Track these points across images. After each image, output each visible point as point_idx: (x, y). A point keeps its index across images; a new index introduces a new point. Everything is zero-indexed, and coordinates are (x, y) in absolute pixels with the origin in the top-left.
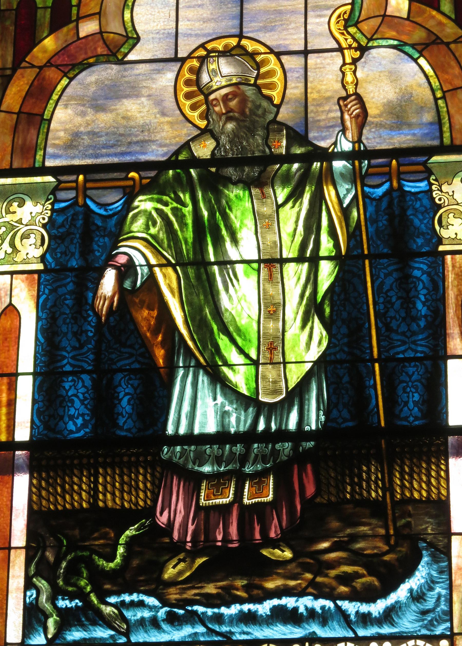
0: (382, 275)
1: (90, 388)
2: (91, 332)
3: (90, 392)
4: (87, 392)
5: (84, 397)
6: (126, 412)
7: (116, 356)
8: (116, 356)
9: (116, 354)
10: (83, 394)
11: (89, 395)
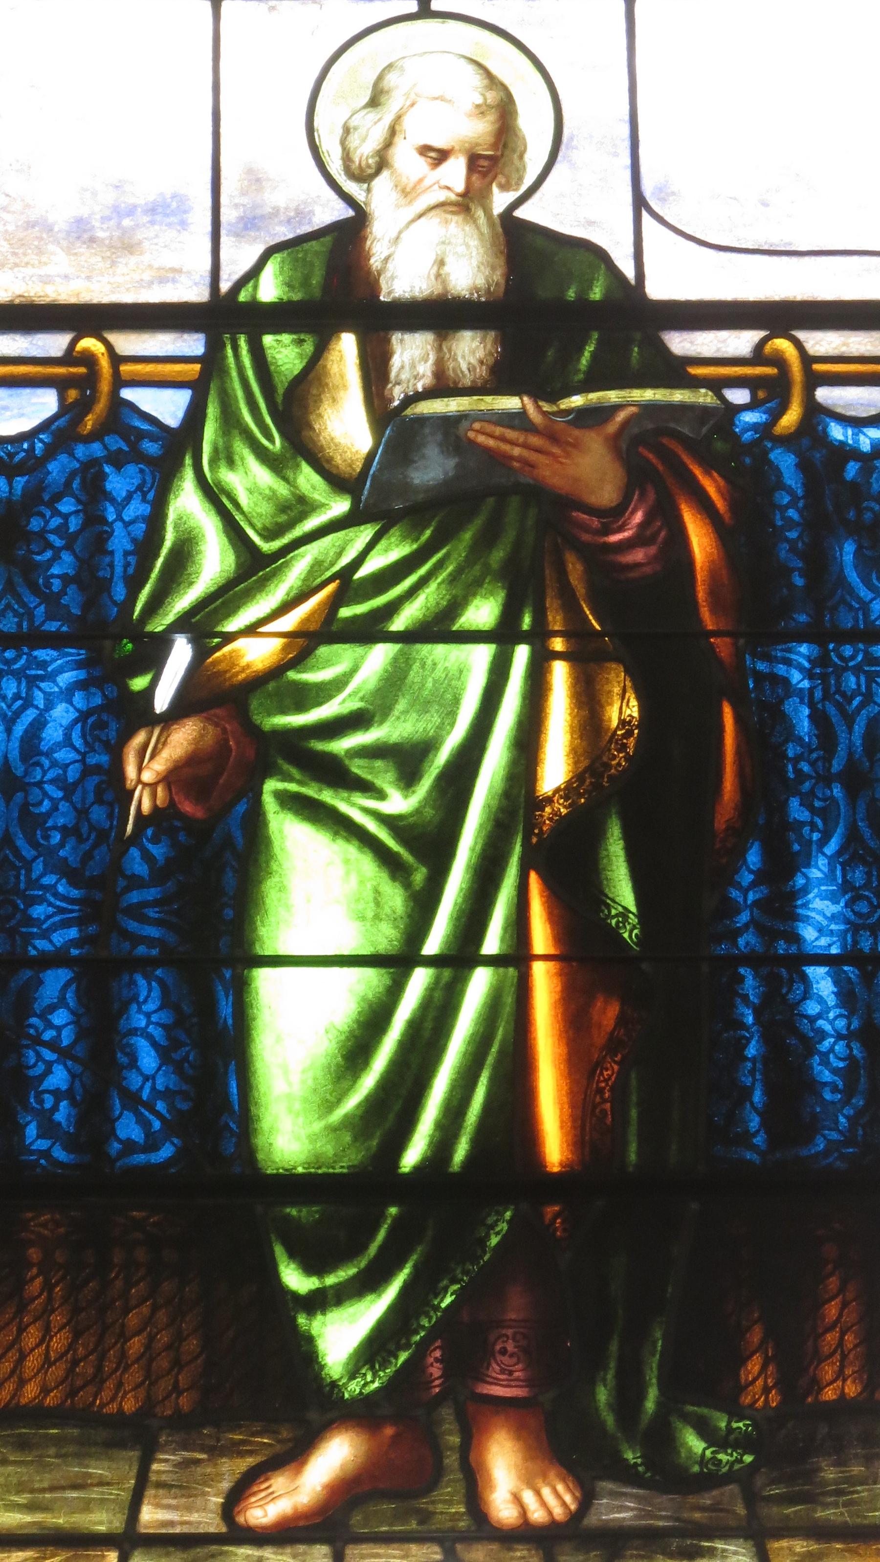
0: (39, 699)
2: (835, 1089)
3: (831, 1015)
6: (92, 828)
9: (50, 904)
11: (831, 1023)
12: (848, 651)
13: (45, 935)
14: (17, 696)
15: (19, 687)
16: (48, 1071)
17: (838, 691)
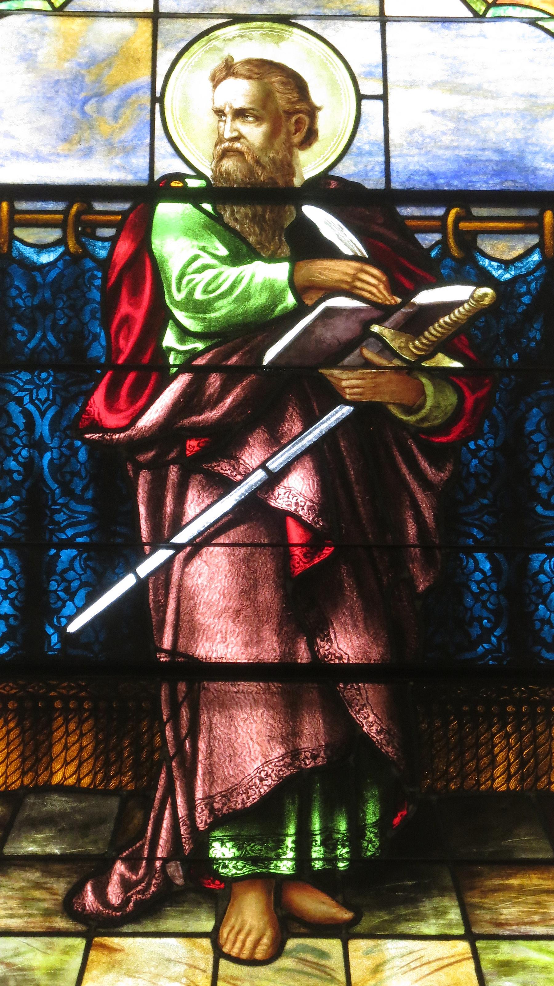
1: (22, 427)
3: (21, 434)
4: (484, 580)
5: (479, 588)
7: (65, 517)
8: (65, 517)
9: (65, 513)
10: (478, 583)
11: (23, 300)
12: (44, 375)
13: (63, 530)
14: (47, 399)
15: (48, 394)
16: (64, 606)
17: (37, 398)
